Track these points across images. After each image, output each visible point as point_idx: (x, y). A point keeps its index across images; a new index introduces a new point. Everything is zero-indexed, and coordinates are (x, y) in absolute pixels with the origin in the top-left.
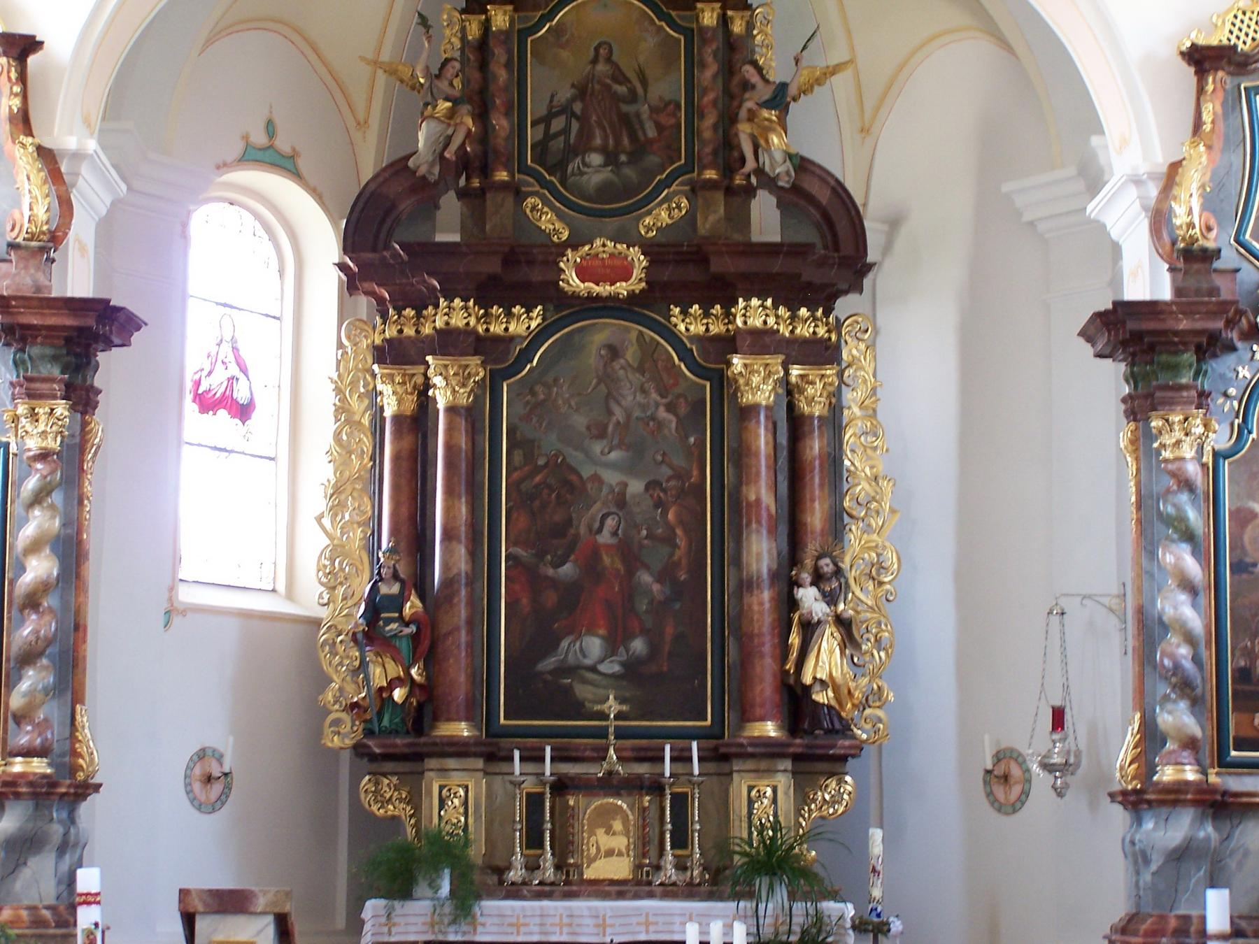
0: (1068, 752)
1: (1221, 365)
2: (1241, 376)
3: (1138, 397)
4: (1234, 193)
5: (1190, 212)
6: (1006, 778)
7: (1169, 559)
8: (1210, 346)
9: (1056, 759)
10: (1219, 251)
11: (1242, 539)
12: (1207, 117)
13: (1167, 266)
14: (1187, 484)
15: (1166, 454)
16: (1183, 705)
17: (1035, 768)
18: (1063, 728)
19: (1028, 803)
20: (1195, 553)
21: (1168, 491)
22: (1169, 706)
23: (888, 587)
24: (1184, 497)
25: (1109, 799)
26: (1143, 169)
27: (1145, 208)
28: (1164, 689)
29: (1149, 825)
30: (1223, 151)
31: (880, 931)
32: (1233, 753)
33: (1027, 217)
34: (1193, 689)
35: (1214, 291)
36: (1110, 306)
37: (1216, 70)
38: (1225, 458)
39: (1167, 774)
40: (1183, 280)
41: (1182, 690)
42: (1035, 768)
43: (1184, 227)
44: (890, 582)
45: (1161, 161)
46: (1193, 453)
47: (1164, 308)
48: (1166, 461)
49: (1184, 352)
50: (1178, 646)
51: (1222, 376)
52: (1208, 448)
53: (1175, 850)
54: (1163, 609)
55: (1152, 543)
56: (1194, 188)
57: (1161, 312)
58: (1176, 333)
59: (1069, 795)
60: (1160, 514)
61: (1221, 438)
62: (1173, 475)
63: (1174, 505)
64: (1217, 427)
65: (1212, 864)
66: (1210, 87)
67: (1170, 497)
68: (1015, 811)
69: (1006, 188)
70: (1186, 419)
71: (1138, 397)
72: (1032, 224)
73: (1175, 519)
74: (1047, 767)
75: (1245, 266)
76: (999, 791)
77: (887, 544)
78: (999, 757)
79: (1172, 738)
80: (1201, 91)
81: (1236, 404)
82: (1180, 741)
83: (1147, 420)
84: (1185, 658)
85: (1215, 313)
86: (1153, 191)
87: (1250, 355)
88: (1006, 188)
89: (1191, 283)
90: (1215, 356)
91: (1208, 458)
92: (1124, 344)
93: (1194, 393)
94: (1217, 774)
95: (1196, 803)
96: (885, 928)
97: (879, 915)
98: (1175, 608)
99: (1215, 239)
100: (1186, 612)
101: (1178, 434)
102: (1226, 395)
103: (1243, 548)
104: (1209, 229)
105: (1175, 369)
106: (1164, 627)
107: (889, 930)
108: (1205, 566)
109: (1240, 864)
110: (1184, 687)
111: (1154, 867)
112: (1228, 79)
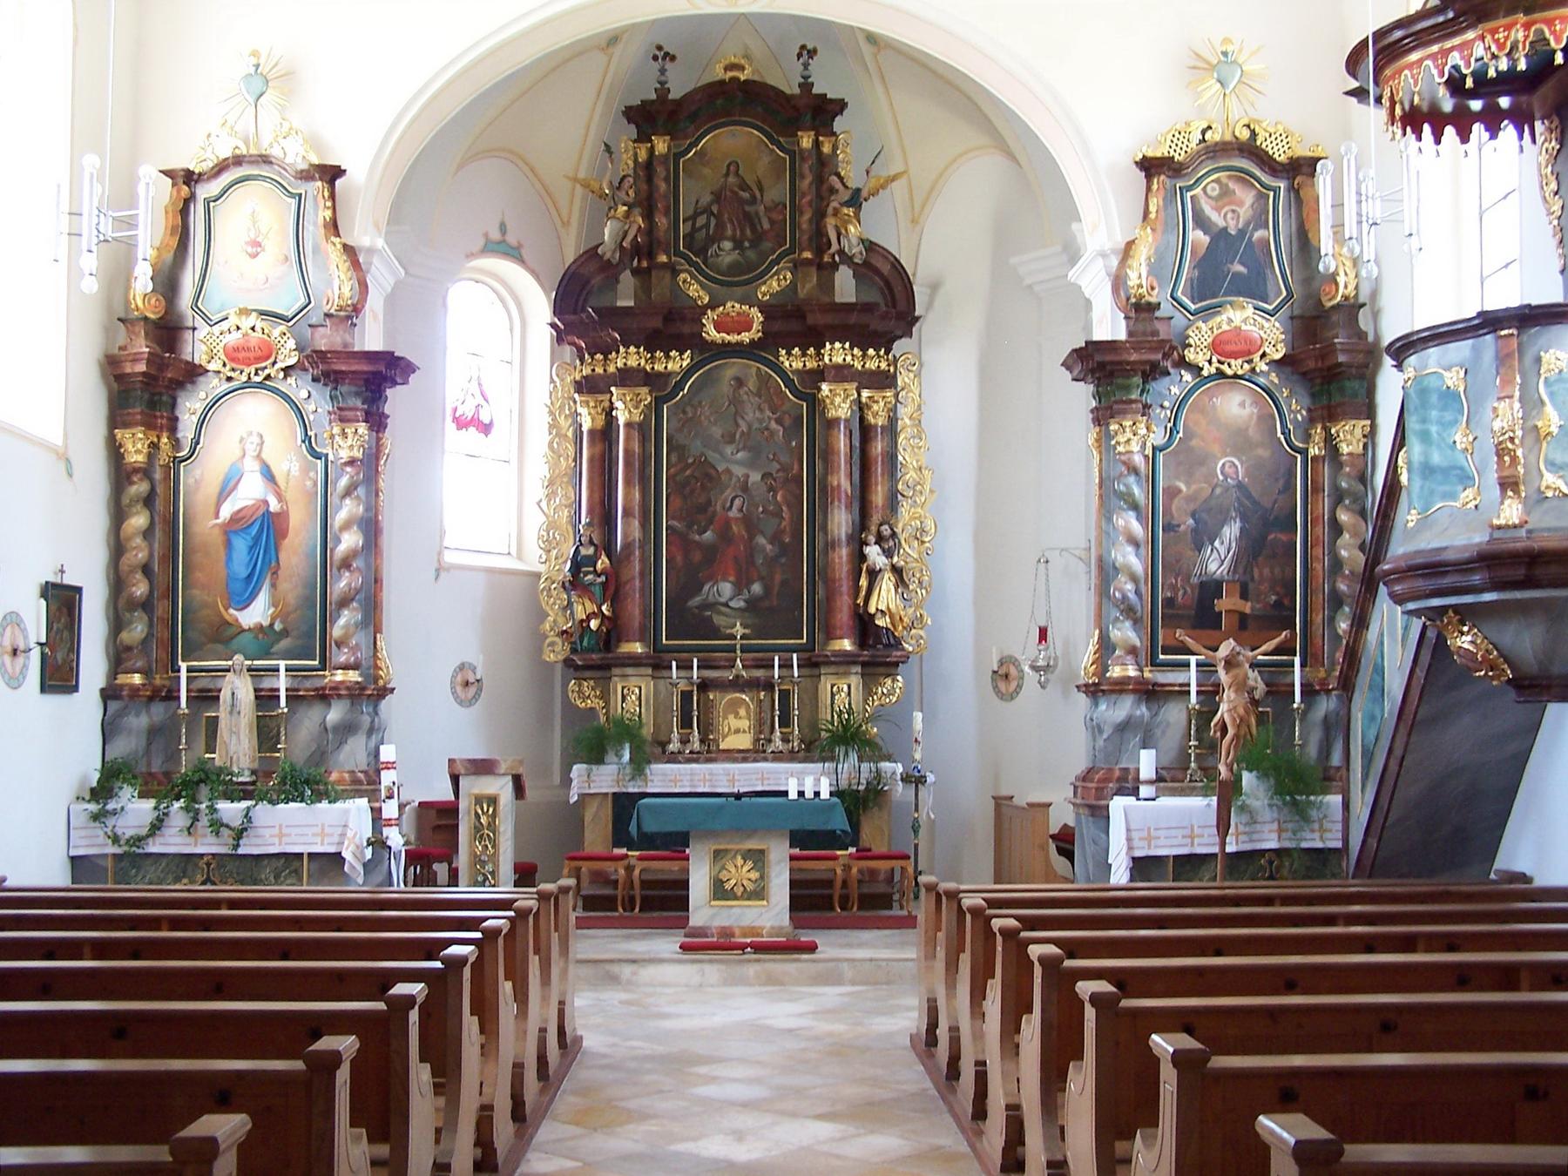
7: (1121, 522)
8: (1153, 372)
9: (1041, 663)
12: (1153, 208)
14: (1134, 471)
15: (1120, 449)
16: (1128, 624)
17: (1026, 669)
21: (1121, 474)
22: (1119, 625)
24: (1132, 479)
26: (1108, 246)
33: (1028, 281)
35: (1155, 333)
39: (1116, 672)
42: (1026, 669)
45: (1120, 242)
51: (1160, 394)
52: (1149, 445)
56: (1143, 258)
58: (1128, 363)
59: (1049, 687)
61: (1158, 437)
62: (1124, 463)
66: (1155, 187)
69: (1013, 260)
72: (1030, 287)
75: (1177, 314)
76: (1002, 686)
78: (1001, 663)
80: (1149, 189)
83: (1108, 425)
86: (1114, 262)
89: (1140, 327)
90: (1155, 379)
91: (1149, 451)
92: (1093, 371)
95: (1134, 691)
100: (1131, 559)
101: (1129, 435)
105: (1127, 389)
108: (1145, 528)
109: (1164, 732)
110: (1129, 611)
111: (1105, 736)
112: (1168, 181)
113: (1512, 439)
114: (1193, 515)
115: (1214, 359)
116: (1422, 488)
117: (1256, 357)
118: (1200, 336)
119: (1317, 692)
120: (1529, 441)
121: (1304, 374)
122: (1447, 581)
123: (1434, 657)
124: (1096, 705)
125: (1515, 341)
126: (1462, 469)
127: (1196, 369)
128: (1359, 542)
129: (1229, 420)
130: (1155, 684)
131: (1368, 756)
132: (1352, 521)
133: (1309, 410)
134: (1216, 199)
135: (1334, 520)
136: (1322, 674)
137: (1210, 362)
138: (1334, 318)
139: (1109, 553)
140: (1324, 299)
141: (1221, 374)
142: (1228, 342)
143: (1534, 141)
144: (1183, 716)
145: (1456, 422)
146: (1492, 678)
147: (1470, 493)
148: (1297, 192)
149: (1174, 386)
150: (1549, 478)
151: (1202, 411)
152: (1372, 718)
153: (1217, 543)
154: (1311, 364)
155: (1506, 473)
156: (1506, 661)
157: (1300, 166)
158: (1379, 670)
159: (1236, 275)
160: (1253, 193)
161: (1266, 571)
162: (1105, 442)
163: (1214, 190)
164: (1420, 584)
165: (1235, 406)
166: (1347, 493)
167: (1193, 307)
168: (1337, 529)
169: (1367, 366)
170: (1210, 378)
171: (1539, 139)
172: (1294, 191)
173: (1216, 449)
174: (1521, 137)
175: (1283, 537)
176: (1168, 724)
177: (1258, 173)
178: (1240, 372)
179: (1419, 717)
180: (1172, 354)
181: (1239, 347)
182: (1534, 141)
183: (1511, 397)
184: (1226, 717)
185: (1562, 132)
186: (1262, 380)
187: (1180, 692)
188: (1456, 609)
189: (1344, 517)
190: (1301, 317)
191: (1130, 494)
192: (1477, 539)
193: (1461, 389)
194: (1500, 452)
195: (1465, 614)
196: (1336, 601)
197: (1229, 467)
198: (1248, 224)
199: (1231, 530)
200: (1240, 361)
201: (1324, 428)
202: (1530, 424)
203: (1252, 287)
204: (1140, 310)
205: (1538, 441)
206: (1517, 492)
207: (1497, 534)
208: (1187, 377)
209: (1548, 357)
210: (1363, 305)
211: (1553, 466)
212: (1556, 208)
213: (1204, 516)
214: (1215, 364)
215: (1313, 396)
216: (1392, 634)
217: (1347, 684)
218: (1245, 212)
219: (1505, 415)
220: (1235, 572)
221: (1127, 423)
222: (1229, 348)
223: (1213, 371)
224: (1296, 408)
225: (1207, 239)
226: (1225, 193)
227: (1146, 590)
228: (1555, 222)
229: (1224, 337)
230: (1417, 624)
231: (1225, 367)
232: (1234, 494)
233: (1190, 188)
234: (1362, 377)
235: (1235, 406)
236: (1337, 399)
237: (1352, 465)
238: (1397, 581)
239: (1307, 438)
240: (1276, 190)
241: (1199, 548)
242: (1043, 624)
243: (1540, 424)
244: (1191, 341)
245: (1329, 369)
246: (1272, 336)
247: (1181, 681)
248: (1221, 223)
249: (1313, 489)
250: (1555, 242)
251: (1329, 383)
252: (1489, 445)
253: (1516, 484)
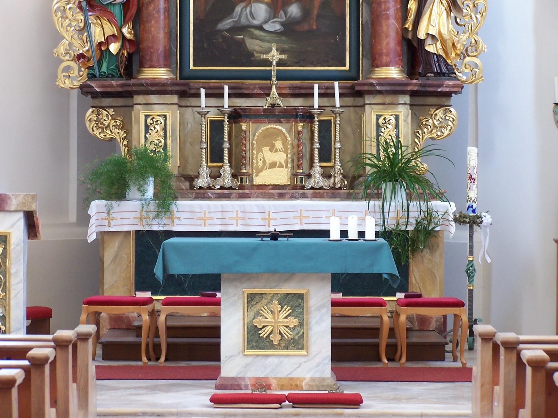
31: (475, 223)
97: (474, 211)
107: (481, 222)
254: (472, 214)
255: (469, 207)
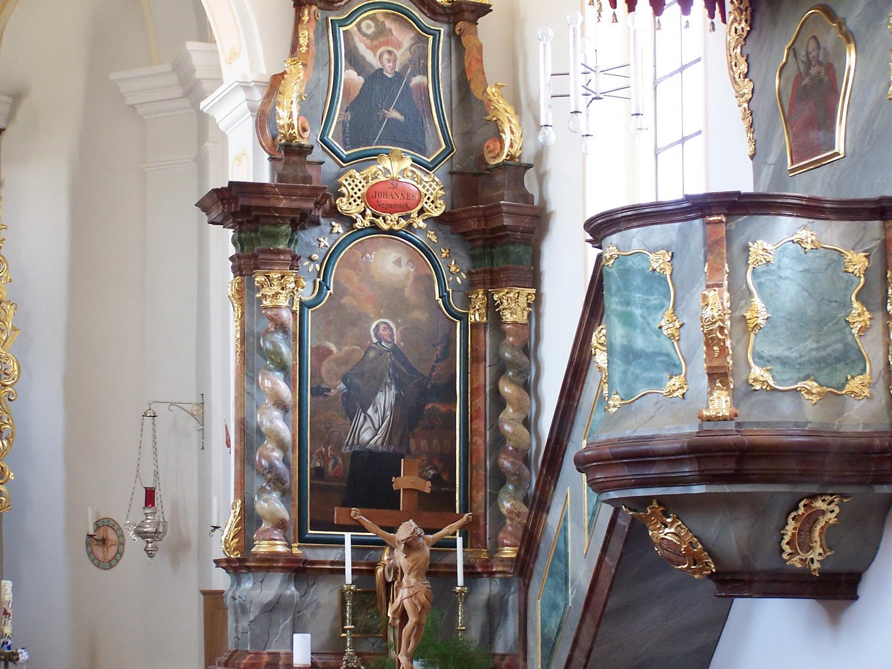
0: (158, 523)
1: (308, 236)
2: (322, 244)
3: (244, 257)
4: (321, 102)
5: (290, 117)
6: (104, 541)
7: (268, 383)
8: (302, 220)
9: (149, 529)
10: (312, 148)
11: (320, 371)
12: (303, 41)
13: (267, 156)
14: (281, 327)
15: (267, 303)
16: (275, 495)
17: (130, 535)
18: (153, 505)
19: (121, 562)
20: (286, 380)
21: (267, 331)
22: (265, 496)
23: (9, 389)
24: (279, 337)
25: (214, 565)
26: (251, 78)
27: (251, 109)
28: (260, 482)
29: (248, 585)
30: (314, 69)
31: (11, 660)
32: (310, 532)
33: (130, 101)
34: (284, 484)
35: (307, 179)
36: (226, 185)
37: (311, 5)
38: (309, 308)
39: (262, 547)
40: (284, 169)
41: (274, 483)
42: (130, 535)
43: (286, 127)
44: (10, 386)
45: (264, 72)
46: (287, 304)
47: (269, 189)
48: (266, 308)
49: (282, 224)
50: (273, 450)
51: (308, 244)
52: (297, 300)
53: (268, 604)
54: (262, 422)
55: (252, 372)
56: (295, 95)
57: (267, 193)
58: (277, 209)
59: (158, 555)
60: (260, 349)
61: (307, 293)
62: (271, 319)
63: (272, 343)
64: (305, 284)
65: (294, 615)
66: (306, 18)
67: (269, 336)
68: (111, 567)
69: (114, 76)
70: (283, 277)
71: (244, 257)
72: (133, 107)
73: (273, 353)
74: (141, 534)
75: (328, 160)
76: (99, 552)
77: (9, 355)
78: (98, 525)
79: (267, 520)
80: (298, 20)
81: (318, 266)
82: (273, 522)
83: (251, 275)
84: (277, 459)
85: (308, 196)
86: (258, 96)
87: (329, 229)
88: (114, 76)
89: (290, 171)
90: (303, 228)
91: (296, 307)
92: (235, 215)
93: (289, 257)
94: (299, 547)
95: (284, 569)
96: (15, 658)
97: (9, 648)
98: (271, 422)
99: (308, 138)
100: (280, 425)
101: (277, 288)
102: (310, 259)
103: (321, 377)
104: (304, 130)
105: (275, 237)
106: (261, 434)
107: (18, 659)
108: (293, 391)
109: (313, 615)
110: (277, 482)
111: (252, 617)
112: (319, 13)
113: (721, 329)
114: (344, 379)
115: (368, 212)
116: (625, 373)
117: (414, 213)
118: (354, 185)
119: (479, 575)
120: (739, 329)
121: (464, 234)
122: (654, 471)
123: (627, 544)
124: (239, 584)
125: (723, 228)
126: (668, 355)
127: (348, 221)
128: (523, 416)
129: (386, 277)
130: (306, 562)
131: (549, 646)
132: (516, 394)
133: (469, 274)
134: (372, 37)
135: (496, 393)
136: (484, 556)
137: (363, 214)
138: (499, 178)
139: (253, 416)
140: (487, 156)
141: (375, 228)
142: (385, 194)
143: (724, 21)
144: (335, 598)
145: (662, 306)
146: (695, 572)
147: (676, 381)
148: (458, 39)
149: (323, 238)
150: (757, 371)
151: (355, 267)
152: (554, 607)
153: (370, 411)
154: (473, 225)
155: (715, 363)
156: (711, 555)
157: (462, 11)
158: (562, 556)
159: (392, 120)
160: (412, 35)
161: (423, 443)
162: (246, 294)
163: (369, 27)
164: (625, 473)
165: (390, 263)
166: (513, 364)
167: (345, 153)
168: (499, 402)
169: (532, 232)
170: (364, 231)
171: (729, 19)
172: (456, 38)
173: (369, 308)
174: (712, 16)
175: (442, 408)
176: (318, 606)
177: (417, 14)
178: (396, 228)
179: (607, 609)
180: (322, 204)
181: (397, 201)
182: (724, 20)
183: (720, 286)
184: (406, 602)
185: (752, 15)
186: (419, 237)
187: (332, 571)
188: (661, 500)
189: (507, 389)
190: (461, 173)
191: (278, 353)
192: (688, 430)
193: (668, 273)
194: (710, 341)
195: (668, 505)
196: (499, 479)
197: (383, 329)
198: (405, 67)
199: (386, 398)
200: (396, 216)
201: (486, 294)
202: (737, 314)
203: (409, 138)
204: (288, 152)
205: (747, 332)
206: (725, 384)
207: (707, 426)
208: (338, 228)
209: (756, 248)
210: (529, 166)
211: (760, 358)
212: (747, 90)
213: (356, 381)
214: (369, 217)
215: (473, 258)
216: (579, 519)
217: (523, 567)
218: (403, 54)
219: (717, 302)
220: (389, 443)
221: (275, 275)
222: (384, 200)
223: (367, 223)
224: (456, 270)
225: (360, 80)
226: (381, 32)
227: (294, 458)
228: (745, 105)
229: (378, 188)
230: (607, 512)
231: (380, 221)
232: (389, 358)
233: (343, 23)
234: (527, 242)
235: (390, 263)
236: (500, 263)
237: (516, 335)
238: (598, 468)
239: (467, 303)
240: (436, 34)
241: (351, 415)
242: (150, 485)
243: (748, 315)
244: (343, 189)
245: (493, 231)
246: (432, 191)
247: (331, 558)
248: (377, 65)
249: (473, 358)
250: (744, 126)
251: (492, 247)
252: (695, 333)
253: (725, 375)
254: (7, 651)
255: (4, 643)
